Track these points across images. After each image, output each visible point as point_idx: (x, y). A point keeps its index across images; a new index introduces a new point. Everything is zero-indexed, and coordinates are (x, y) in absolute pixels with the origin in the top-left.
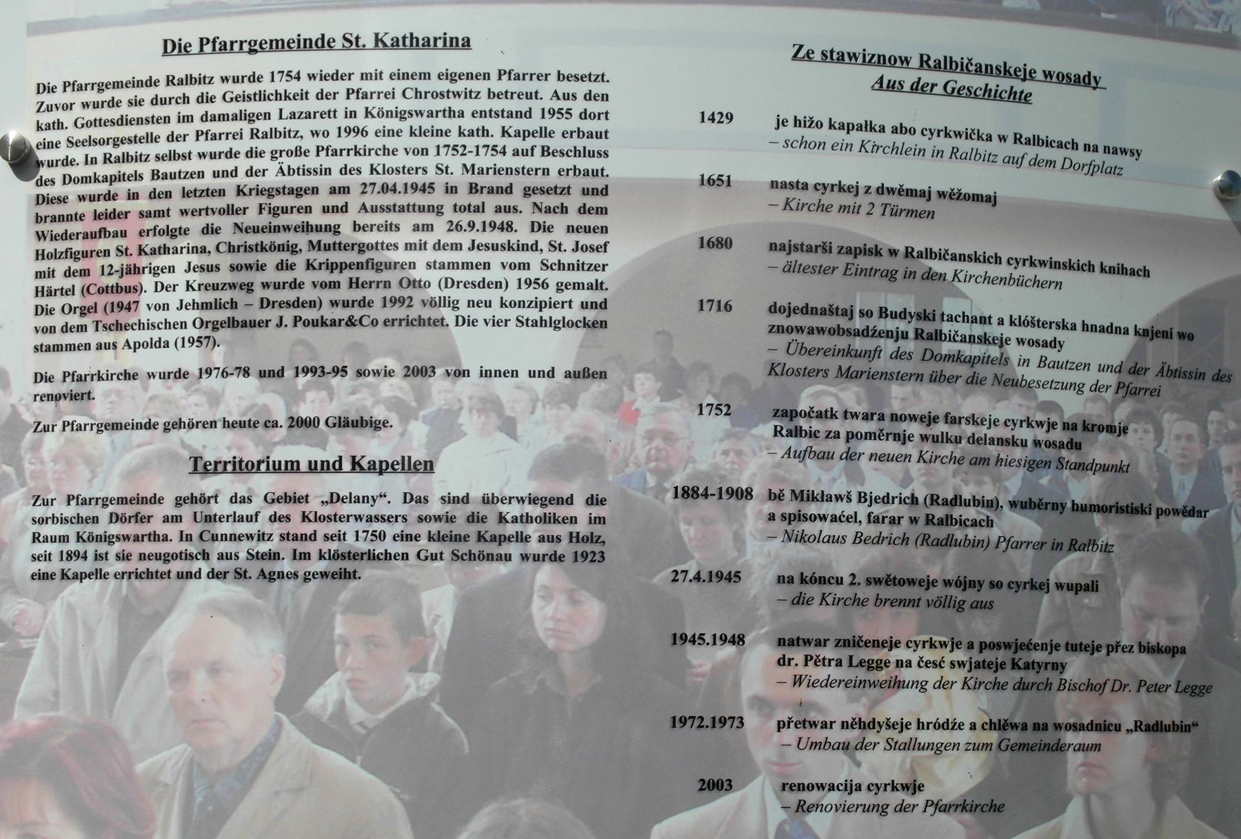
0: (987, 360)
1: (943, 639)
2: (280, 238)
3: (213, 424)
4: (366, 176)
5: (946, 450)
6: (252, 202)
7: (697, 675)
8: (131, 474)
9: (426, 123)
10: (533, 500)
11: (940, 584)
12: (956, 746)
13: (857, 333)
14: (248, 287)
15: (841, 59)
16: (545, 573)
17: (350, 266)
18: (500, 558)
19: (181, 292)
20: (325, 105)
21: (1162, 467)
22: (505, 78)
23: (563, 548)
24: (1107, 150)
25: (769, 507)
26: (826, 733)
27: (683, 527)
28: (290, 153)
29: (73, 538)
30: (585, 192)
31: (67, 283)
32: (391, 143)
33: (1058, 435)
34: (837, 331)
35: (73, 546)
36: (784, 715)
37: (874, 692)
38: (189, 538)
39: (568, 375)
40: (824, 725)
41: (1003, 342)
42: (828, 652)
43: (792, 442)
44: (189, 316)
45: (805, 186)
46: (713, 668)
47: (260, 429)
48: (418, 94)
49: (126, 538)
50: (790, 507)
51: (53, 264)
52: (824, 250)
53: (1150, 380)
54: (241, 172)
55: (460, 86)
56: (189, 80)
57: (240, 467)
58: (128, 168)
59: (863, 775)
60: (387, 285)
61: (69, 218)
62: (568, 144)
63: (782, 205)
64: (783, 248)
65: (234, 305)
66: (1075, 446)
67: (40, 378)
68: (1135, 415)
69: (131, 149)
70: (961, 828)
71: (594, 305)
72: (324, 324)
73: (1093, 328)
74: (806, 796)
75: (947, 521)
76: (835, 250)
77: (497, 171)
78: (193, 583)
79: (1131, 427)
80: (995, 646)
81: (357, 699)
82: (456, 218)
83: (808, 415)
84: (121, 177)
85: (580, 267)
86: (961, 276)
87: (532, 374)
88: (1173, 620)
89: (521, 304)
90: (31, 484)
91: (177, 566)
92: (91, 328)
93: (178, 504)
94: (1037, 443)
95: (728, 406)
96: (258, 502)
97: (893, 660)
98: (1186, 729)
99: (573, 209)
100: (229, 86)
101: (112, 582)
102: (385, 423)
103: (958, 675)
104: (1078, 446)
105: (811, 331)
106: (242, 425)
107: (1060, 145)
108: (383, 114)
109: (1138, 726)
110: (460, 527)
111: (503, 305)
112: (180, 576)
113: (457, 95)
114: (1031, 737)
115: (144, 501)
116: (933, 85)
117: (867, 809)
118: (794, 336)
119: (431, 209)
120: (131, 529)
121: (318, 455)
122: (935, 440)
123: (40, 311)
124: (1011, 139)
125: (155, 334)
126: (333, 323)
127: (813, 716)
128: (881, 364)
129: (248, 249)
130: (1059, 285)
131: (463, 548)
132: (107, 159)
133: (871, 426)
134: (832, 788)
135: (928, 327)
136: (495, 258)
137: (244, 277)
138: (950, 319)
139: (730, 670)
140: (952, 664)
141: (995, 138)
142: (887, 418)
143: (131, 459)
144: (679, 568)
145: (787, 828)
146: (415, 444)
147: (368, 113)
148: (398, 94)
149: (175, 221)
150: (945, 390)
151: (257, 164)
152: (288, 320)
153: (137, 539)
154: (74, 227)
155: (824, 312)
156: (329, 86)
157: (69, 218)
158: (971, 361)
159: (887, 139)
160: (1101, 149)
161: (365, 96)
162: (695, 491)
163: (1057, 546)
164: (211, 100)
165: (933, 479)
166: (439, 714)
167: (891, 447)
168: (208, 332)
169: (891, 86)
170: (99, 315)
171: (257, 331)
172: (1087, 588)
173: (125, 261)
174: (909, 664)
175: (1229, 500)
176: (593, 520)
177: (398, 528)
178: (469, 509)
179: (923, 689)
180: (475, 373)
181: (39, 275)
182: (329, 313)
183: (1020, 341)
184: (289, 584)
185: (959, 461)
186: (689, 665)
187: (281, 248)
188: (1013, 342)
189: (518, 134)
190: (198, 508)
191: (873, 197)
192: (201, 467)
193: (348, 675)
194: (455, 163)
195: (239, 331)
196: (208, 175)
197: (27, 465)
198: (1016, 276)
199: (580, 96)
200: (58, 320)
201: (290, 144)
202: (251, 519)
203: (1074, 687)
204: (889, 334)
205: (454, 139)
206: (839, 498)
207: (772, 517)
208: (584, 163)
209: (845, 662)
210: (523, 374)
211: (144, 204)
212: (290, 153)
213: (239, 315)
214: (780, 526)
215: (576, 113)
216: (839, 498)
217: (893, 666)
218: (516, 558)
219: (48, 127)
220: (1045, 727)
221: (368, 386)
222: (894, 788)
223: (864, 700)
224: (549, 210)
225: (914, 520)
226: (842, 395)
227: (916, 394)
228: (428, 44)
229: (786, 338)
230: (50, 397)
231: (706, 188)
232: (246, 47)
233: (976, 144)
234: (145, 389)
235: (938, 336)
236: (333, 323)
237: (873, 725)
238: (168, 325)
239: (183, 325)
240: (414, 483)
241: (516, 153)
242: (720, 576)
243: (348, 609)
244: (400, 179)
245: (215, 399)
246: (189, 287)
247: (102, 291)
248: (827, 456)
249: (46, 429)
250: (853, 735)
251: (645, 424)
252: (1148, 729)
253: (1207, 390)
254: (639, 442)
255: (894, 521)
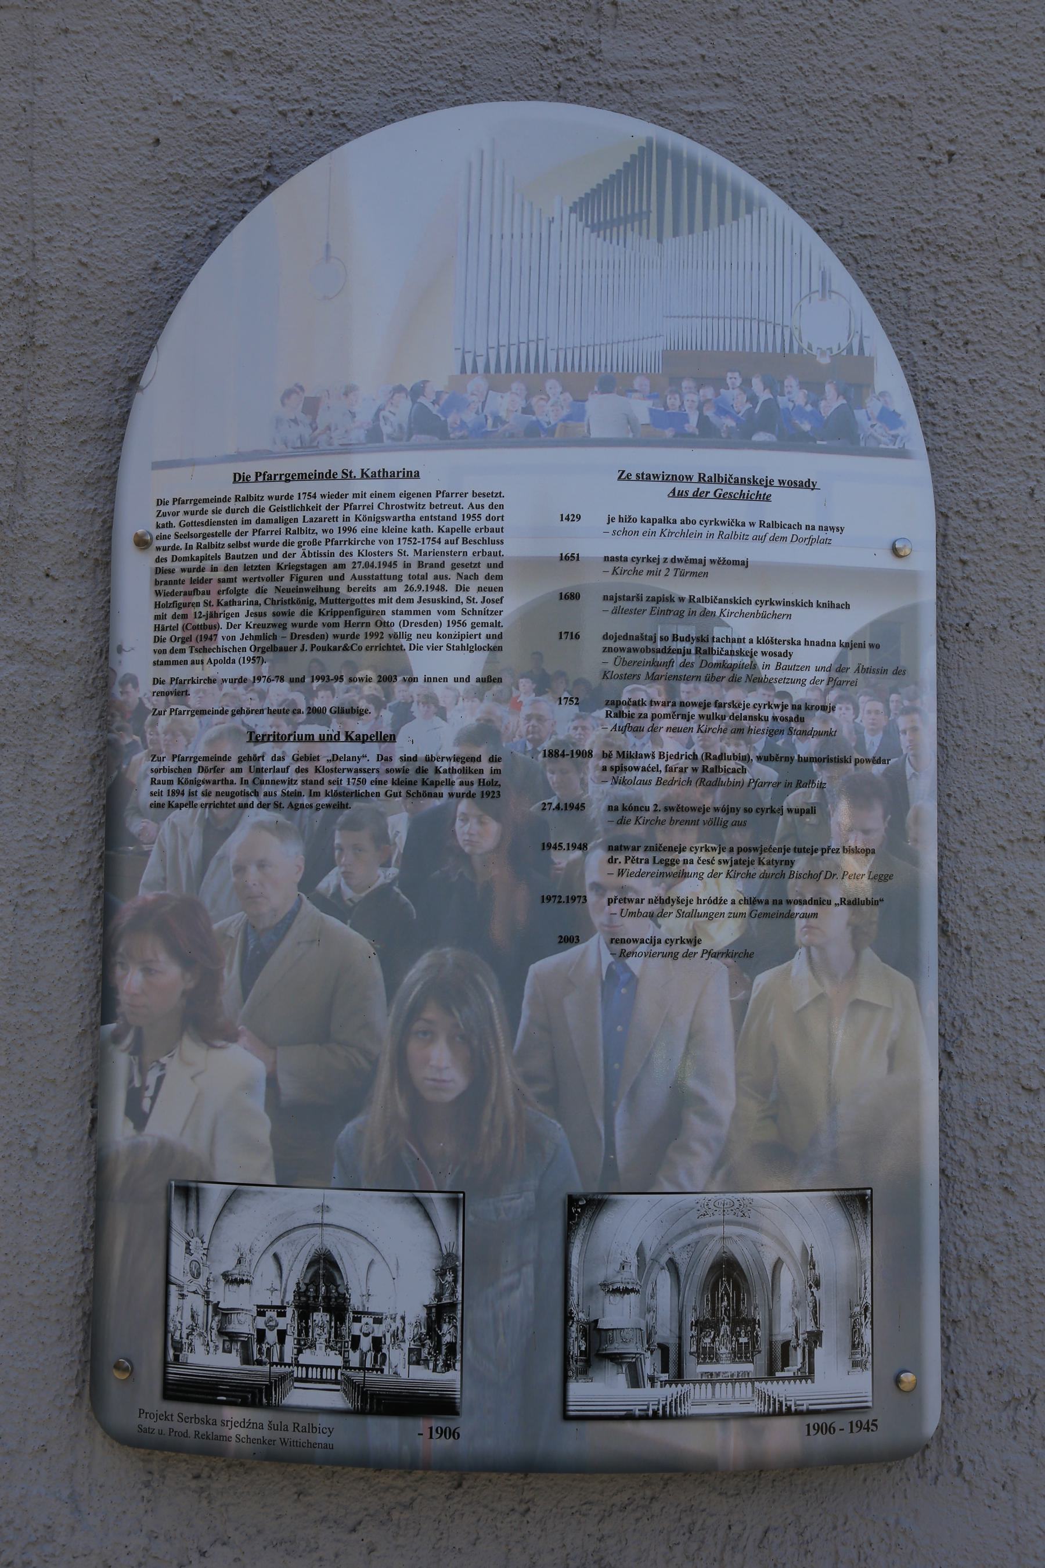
0: (742, 666)
1: (713, 845)
2: (303, 596)
3: (262, 711)
4: (356, 558)
5: (715, 724)
6: (286, 574)
7: (558, 869)
8: (211, 742)
9: (392, 524)
10: (456, 759)
11: (712, 810)
12: (722, 914)
13: (659, 651)
14: (284, 627)
15: (648, 478)
16: (464, 805)
17: (345, 613)
18: (436, 795)
19: (243, 630)
20: (331, 514)
21: (859, 732)
22: (440, 496)
23: (475, 789)
24: (821, 528)
25: (602, 762)
26: (639, 906)
27: (549, 775)
28: (309, 543)
29: (176, 782)
30: (489, 566)
31: (174, 623)
32: (371, 536)
33: (789, 713)
34: (647, 650)
35: (175, 787)
36: (612, 895)
37: (669, 880)
38: (246, 782)
39: (478, 680)
40: (638, 901)
41: (752, 654)
42: (640, 855)
43: (617, 721)
44: (248, 644)
45: (626, 559)
46: (568, 865)
47: (290, 714)
48: (387, 507)
49: (208, 782)
50: (616, 762)
51: (165, 611)
52: (638, 600)
53: (850, 676)
54: (280, 555)
55: (413, 501)
56: (249, 498)
57: (278, 738)
58: (211, 552)
59: (663, 934)
60: (368, 625)
61: (176, 582)
62: (479, 536)
63: (611, 571)
64: (612, 598)
65: (275, 637)
66: (800, 720)
67: (157, 681)
68: (840, 699)
69: (214, 540)
70: (725, 967)
71: (494, 637)
72: (329, 649)
73: (812, 643)
74: (625, 946)
75: (716, 769)
76: (644, 599)
77: (436, 554)
78: (248, 811)
79: (837, 707)
80: (748, 850)
81: (348, 884)
82: (410, 583)
83: (627, 704)
84: (207, 558)
85: (486, 612)
86: (725, 613)
87: (456, 680)
88: (866, 832)
89: (450, 636)
90: (151, 747)
91: (239, 800)
92: (188, 651)
93: (240, 761)
94: (775, 718)
95: (577, 699)
96: (288, 760)
97: (681, 859)
98: (876, 903)
99: (481, 576)
100: (274, 502)
101: (199, 810)
102: (366, 711)
103: (723, 869)
104: (802, 720)
105: (629, 650)
106: (279, 712)
107: (790, 527)
108: (367, 519)
109: (843, 901)
110: (412, 776)
111: (438, 637)
112: (241, 806)
113: (411, 507)
114: (771, 909)
115: (220, 759)
116: (708, 493)
117: (664, 955)
118: (619, 654)
119: (395, 577)
120: (210, 776)
121: (324, 731)
122: (709, 718)
123: (158, 640)
124: (757, 524)
125: (227, 655)
126: (335, 649)
127: (631, 895)
128: (675, 670)
129: (284, 603)
130: (789, 616)
131: (413, 789)
132: (199, 547)
133: (667, 710)
134: (642, 941)
135: (704, 646)
136: (434, 608)
137: (281, 620)
138: (718, 640)
139: (578, 867)
140: (720, 862)
141: (747, 524)
142: (678, 705)
143: (212, 732)
144: (547, 801)
145: (614, 967)
146: (384, 724)
147: (357, 518)
148: (375, 506)
149: (239, 585)
150: (715, 686)
151: (290, 550)
152: (307, 647)
153: (214, 783)
154: (179, 588)
155: (637, 638)
156: (334, 502)
157: (176, 582)
158: (732, 667)
159: (677, 528)
160: (817, 528)
161: (355, 508)
162: (557, 753)
163: (788, 785)
164: (262, 510)
165: (707, 743)
166: (398, 894)
167: (680, 723)
168: (259, 654)
169: (681, 495)
170: (192, 644)
171: (290, 654)
172: (808, 812)
173: (209, 609)
174: (692, 862)
175: (904, 752)
176: (493, 772)
177: (374, 776)
178: (417, 764)
179: (701, 878)
180: (421, 679)
181: (157, 617)
182: (333, 642)
183: (764, 653)
184: (308, 812)
185: (724, 731)
186: (552, 863)
187: (303, 602)
188: (759, 654)
189: (448, 530)
190: (252, 764)
191: (669, 565)
192: (254, 738)
193: (343, 869)
194: (410, 549)
195: (279, 654)
196: (260, 556)
197: (148, 736)
198: (761, 612)
199: (486, 506)
200: (168, 646)
201: (309, 538)
202: (285, 770)
203: (799, 876)
204: (679, 651)
205: (409, 534)
206: (647, 756)
207: (604, 769)
208: (488, 548)
209: (651, 861)
210: (451, 680)
211: (221, 574)
212: (309, 543)
213: (279, 643)
214: (609, 774)
215: (483, 517)
216: (647, 756)
217: (681, 863)
218: (446, 795)
219: (163, 526)
220: (781, 903)
221: (356, 688)
222: (682, 942)
223: (663, 885)
224: (466, 578)
225: (695, 770)
226: (649, 691)
227: (696, 689)
228: (393, 475)
229: (614, 655)
230: (162, 693)
231: (564, 562)
232: (283, 478)
233: (734, 528)
234: (221, 689)
235: (710, 652)
236: (335, 649)
237: (669, 901)
238: (235, 649)
239: (244, 649)
240: (384, 748)
241: (447, 542)
242: (572, 806)
243: (344, 827)
244: (376, 559)
245: (263, 695)
246: (248, 626)
247: (196, 628)
248: (638, 730)
249: (160, 714)
250: (655, 908)
251: (525, 710)
252: (849, 903)
253: (889, 681)
254: (522, 723)
255: (682, 770)
